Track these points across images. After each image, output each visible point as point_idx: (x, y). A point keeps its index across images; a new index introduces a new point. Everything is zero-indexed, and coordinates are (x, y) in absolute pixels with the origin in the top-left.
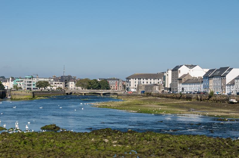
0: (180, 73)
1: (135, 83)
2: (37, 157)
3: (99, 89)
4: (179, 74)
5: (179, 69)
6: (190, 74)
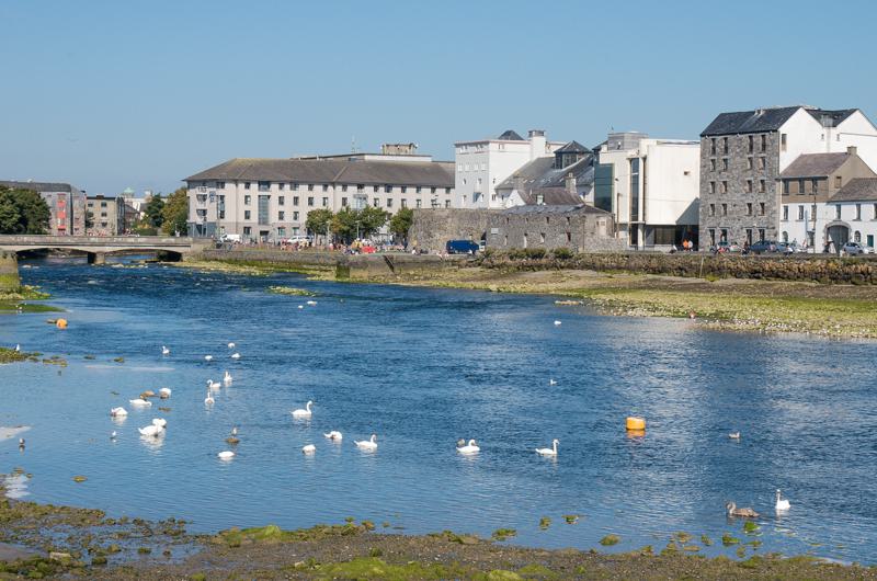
0: (784, 149)
1: (246, 202)
2: (299, 578)
3: (19, 231)
4: (782, 154)
5: (782, 130)
6: (858, 153)
